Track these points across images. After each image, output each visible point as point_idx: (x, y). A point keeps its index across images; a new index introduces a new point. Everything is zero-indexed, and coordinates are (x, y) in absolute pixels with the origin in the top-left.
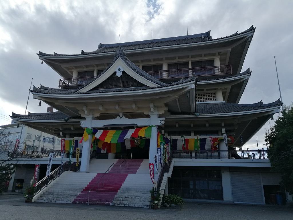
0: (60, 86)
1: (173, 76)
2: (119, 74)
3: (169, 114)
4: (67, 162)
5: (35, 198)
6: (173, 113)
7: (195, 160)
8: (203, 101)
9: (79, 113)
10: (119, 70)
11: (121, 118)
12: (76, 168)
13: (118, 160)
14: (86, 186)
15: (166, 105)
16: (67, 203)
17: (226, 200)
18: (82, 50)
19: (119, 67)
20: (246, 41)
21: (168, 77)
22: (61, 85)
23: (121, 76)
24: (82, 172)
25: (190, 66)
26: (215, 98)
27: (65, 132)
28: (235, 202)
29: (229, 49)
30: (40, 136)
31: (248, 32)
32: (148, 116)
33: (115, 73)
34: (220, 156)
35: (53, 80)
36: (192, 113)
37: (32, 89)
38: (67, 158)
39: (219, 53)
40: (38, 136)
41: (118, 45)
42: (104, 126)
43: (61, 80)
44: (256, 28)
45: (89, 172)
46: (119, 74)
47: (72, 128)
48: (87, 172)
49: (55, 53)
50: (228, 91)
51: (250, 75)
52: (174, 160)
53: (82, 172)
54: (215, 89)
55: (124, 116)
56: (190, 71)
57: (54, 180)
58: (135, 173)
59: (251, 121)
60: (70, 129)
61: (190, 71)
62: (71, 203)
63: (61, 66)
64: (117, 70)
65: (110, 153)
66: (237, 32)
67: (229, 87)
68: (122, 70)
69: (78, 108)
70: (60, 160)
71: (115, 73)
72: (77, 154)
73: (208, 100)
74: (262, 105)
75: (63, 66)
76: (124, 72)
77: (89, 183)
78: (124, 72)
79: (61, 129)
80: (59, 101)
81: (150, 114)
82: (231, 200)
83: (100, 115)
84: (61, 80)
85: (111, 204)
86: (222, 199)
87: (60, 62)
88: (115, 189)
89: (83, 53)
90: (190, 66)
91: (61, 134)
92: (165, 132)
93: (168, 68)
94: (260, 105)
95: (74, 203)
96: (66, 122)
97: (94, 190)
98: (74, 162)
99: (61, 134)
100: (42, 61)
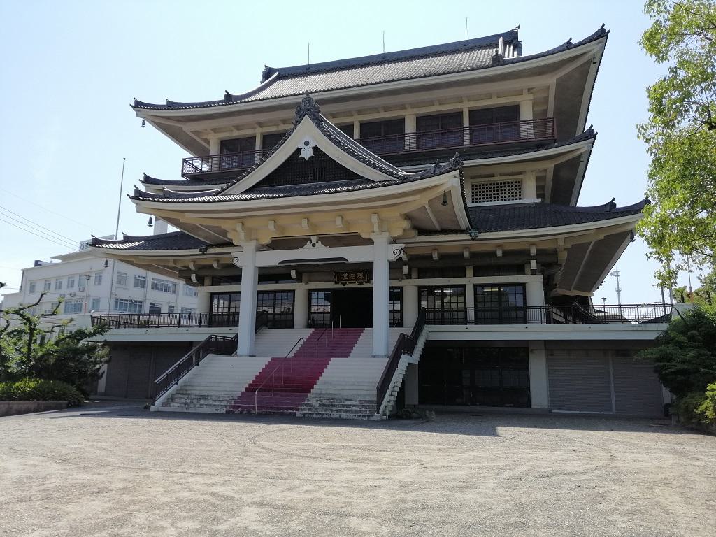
0: (183, 175)
1: (430, 144)
2: (307, 154)
3: (414, 233)
4: (210, 337)
5: (153, 408)
6: (423, 231)
7: (472, 327)
8: (496, 199)
9: (229, 236)
10: (307, 143)
11: (314, 245)
12: (228, 347)
13: (313, 329)
14: (255, 379)
15: (407, 217)
16: (217, 412)
17: (535, 407)
18: (226, 91)
19: (305, 138)
20: (588, 63)
21: (418, 147)
22: (186, 172)
23: (311, 158)
24: (241, 356)
25: (466, 123)
26: (520, 192)
27: (203, 273)
28: (553, 411)
29: (551, 81)
30: (144, 278)
31: (591, 41)
32: (370, 242)
33: (299, 150)
34: (659, 313)
35: (169, 160)
36: (462, 232)
37: (132, 194)
38: (209, 327)
39: (529, 90)
40: (142, 277)
41: (307, 69)
42: (282, 262)
43: (184, 160)
44: (609, 31)
45: (255, 356)
46: (307, 154)
47: (215, 266)
48: (250, 356)
49: (169, 102)
50: (550, 176)
51: (594, 142)
52: (427, 328)
53: (241, 356)
54: (520, 173)
55: (320, 242)
56: (466, 134)
57: (188, 371)
58: (346, 356)
59: (593, 243)
60: (211, 267)
61: (466, 134)
62: (224, 412)
63: (184, 129)
64: (301, 145)
65: (529, 251)
66: (571, 39)
67: (550, 166)
68: (312, 144)
69: (225, 225)
70: (201, 334)
71: (299, 150)
72: (231, 320)
73: (511, 198)
74: (613, 210)
75: (188, 128)
76: (316, 149)
77: (257, 377)
78: (316, 149)
79: (192, 267)
80: (187, 215)
81: (372, 236)
82: (546, 408)
83: (273, 241)
84: (184, 160)
85: (298, 414)
86: (529, 405)
87: (181, 121)
88: (305, 386)
89: (229, 97)
90: (466, 123)
91: (193, 277)
92: (410, 269)
93: (418, 128)
94: (609, 210)
95: (228, 412)
96: (203, 254)
97: (265, 390)
98: (216, 336)
99: (193, 277)
100: (144, 121)
